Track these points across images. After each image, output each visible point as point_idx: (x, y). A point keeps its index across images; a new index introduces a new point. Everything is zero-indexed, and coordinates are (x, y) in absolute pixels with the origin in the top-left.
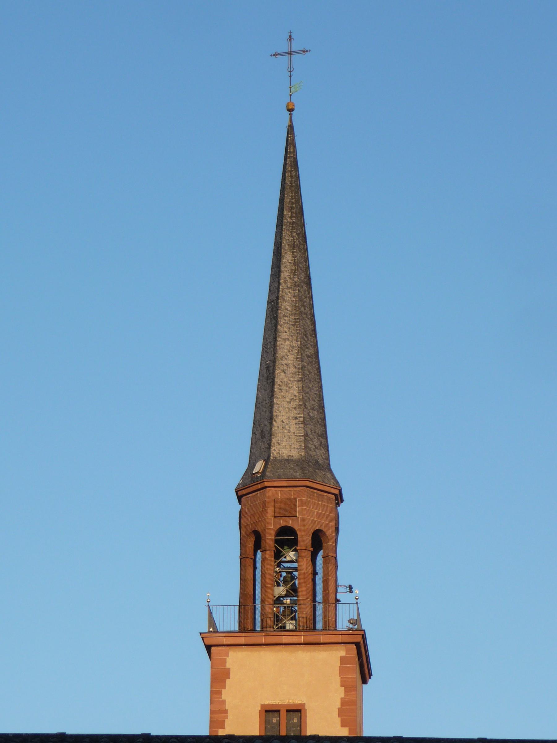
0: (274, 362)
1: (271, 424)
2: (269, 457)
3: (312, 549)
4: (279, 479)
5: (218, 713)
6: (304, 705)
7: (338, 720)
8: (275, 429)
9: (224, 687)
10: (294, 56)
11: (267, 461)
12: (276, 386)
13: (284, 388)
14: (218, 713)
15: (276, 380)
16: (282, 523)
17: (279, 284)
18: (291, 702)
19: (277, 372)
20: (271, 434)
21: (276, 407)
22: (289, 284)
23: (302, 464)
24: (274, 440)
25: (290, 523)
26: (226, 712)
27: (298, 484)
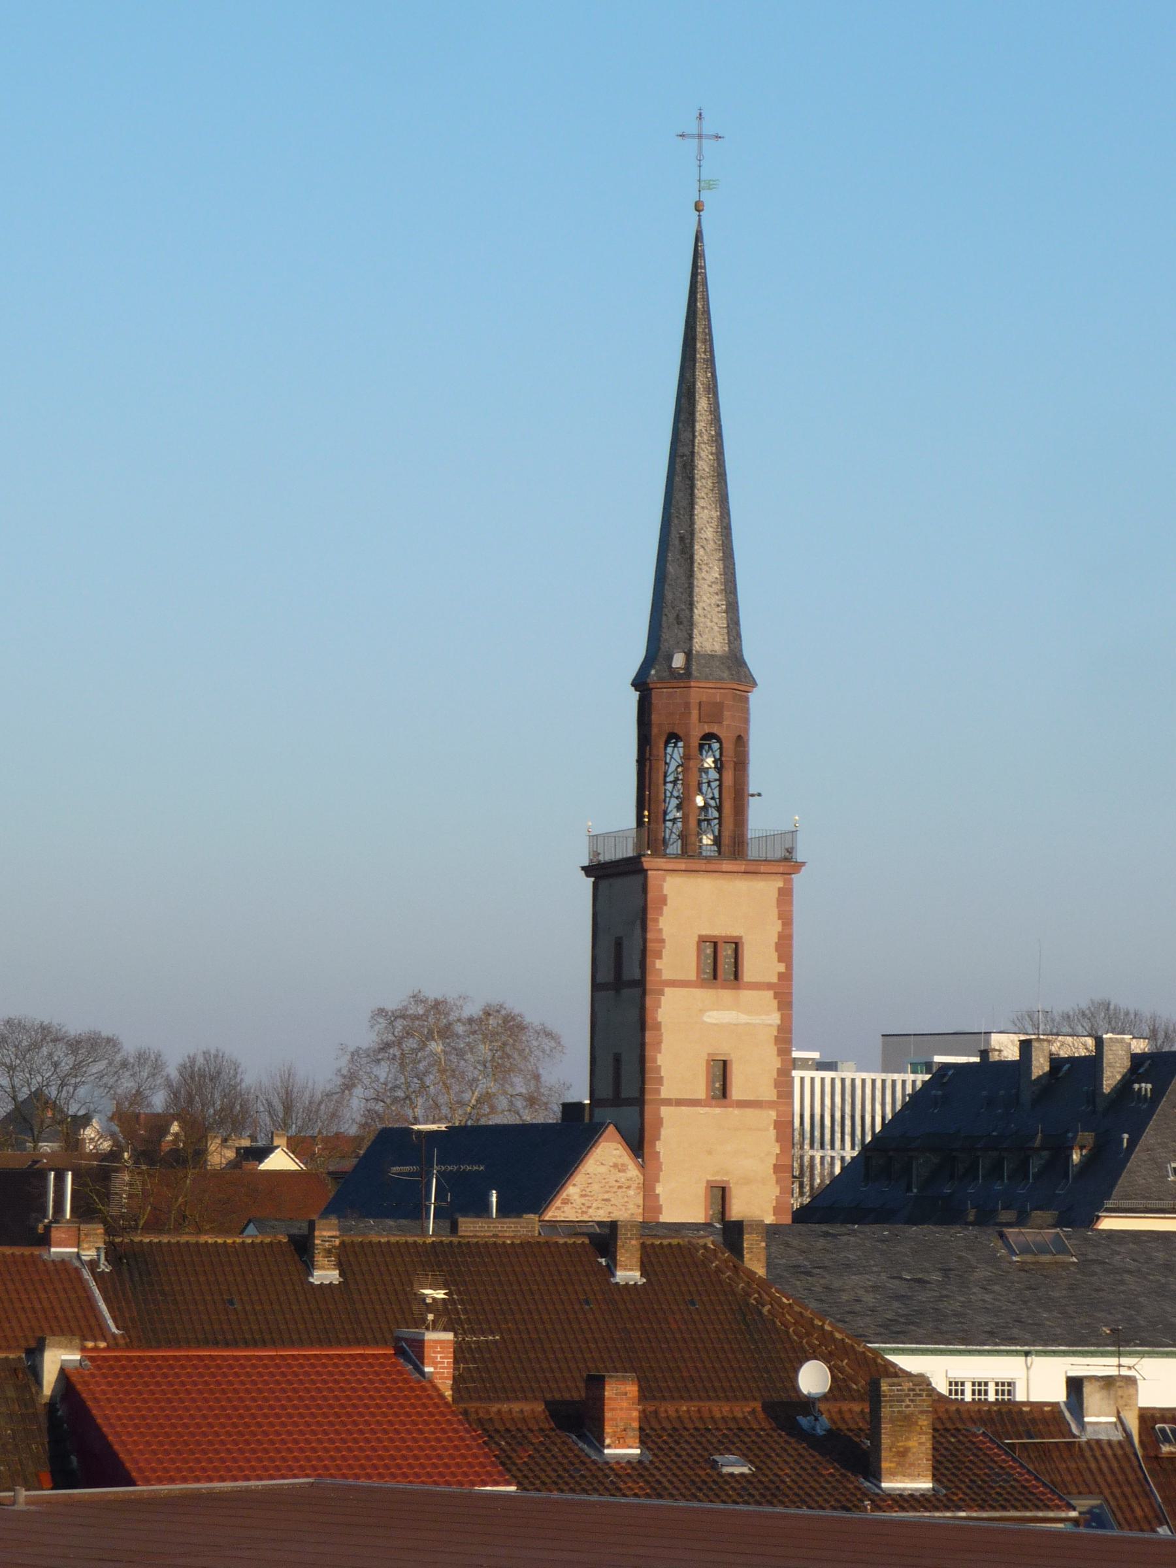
0: (692, 533)
1: (691, 610)
2: (690, 650)
3: (1040, 1066)
4: (707, 678)
5: (668, 1102)
6: (741, 938)
7: (775, 955)
8: (696, 617)
9: (661, 914)
10: (696, 132)
11: (689, 655)
12: (696, 565)
13: (704, 567)
14: (668, 1102)
15: (696, 557)
16: (707, 729)
17: (694, 437)
18: (729, 934)
19: (696, 547)
20: (691, 624)
21: (696, 590)
22: (705, 437)
23: (723, 659)
24: (695, 631)
25: (715, 729)
26: (663, 941)
27: (724, 686)
